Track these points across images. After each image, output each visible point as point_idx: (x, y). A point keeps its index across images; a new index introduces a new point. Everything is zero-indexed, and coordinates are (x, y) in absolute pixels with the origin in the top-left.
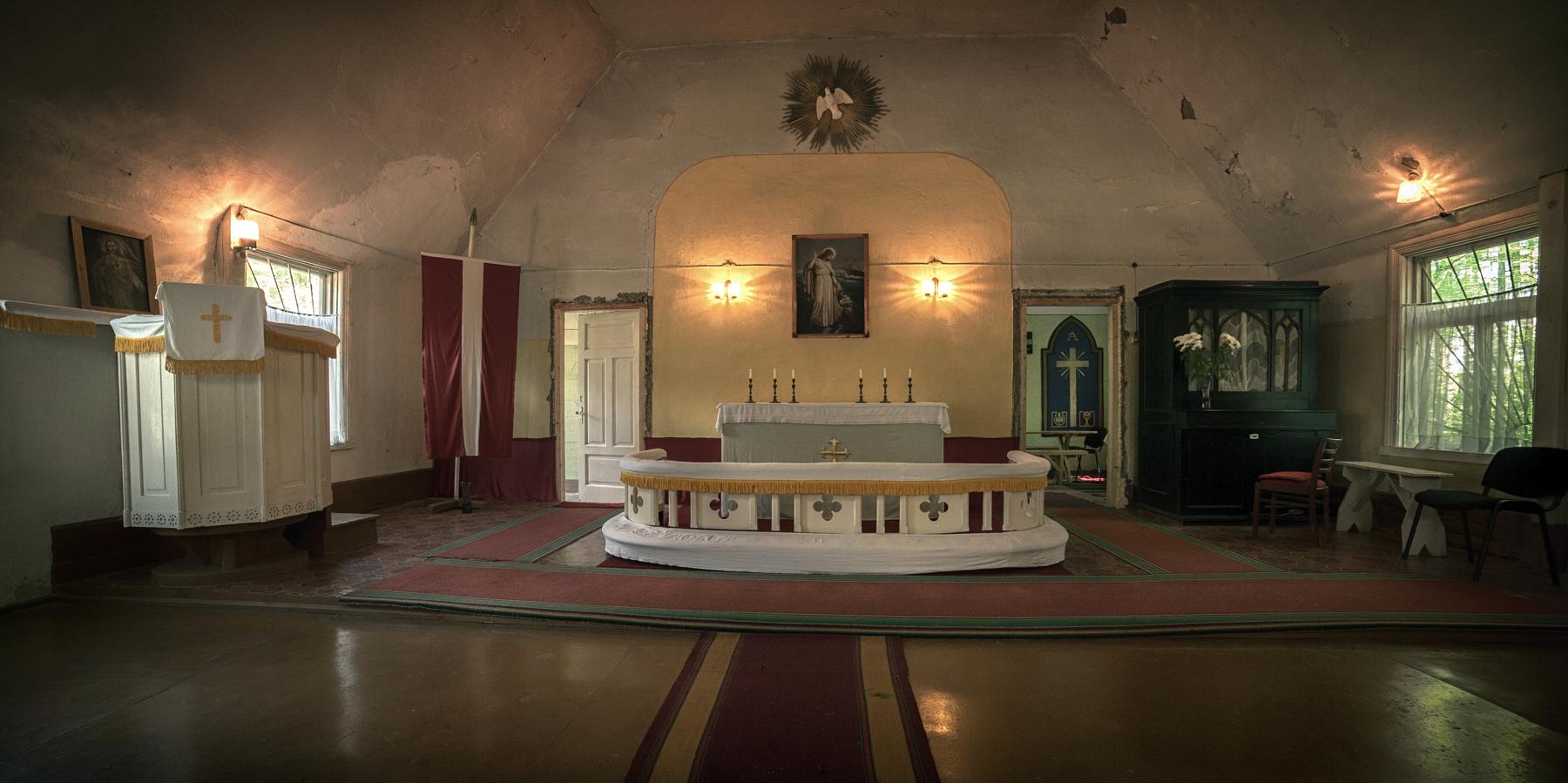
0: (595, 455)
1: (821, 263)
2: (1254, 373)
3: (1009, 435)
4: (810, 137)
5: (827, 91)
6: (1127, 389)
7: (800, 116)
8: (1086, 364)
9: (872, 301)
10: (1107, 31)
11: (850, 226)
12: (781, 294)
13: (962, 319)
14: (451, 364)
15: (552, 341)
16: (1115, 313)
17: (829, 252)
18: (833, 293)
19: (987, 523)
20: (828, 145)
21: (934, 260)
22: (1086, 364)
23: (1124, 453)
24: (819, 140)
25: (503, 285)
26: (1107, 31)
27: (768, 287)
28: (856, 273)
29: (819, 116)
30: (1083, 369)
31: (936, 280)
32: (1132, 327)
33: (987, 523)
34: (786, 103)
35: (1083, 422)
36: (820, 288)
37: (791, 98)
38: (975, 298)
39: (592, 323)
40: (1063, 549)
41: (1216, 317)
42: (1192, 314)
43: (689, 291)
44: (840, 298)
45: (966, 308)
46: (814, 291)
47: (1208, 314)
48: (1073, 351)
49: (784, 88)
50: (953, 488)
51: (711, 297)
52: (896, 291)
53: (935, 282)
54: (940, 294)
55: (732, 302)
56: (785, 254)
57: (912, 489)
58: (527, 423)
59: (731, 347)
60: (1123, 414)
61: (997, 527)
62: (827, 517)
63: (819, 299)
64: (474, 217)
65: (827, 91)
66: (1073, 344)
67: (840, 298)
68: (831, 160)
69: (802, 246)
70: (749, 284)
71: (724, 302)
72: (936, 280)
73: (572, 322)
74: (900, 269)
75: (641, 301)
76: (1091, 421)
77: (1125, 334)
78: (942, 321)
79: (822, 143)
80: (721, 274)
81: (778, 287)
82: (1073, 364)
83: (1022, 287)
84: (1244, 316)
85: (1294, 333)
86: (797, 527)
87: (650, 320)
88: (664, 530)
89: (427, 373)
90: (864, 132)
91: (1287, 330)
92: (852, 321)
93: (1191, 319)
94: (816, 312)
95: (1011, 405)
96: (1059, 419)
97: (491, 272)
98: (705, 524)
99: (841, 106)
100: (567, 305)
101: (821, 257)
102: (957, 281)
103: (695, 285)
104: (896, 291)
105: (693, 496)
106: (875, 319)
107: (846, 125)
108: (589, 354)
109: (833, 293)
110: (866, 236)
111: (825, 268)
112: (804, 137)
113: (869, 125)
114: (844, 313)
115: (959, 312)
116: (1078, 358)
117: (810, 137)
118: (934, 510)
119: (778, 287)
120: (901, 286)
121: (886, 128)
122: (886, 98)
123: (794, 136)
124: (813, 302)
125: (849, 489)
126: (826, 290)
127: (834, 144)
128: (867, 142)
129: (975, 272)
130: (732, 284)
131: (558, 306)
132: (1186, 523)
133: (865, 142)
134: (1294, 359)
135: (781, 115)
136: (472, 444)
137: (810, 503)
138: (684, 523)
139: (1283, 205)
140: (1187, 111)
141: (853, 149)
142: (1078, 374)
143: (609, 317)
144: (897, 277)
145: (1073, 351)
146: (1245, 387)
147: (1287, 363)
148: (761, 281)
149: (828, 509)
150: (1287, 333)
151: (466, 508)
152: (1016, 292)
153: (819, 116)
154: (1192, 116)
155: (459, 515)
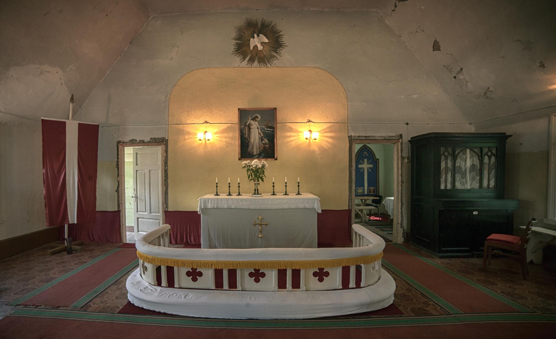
0: (139, 220)
1: (252, 122)
2: (473, 179)
3: (347, 208)
4: (247, 59)
5: (255, 35)
6: (404, 185)
7: (242, 48)
8: (371, 166)
9: (279, 141)
10: (396, 6)
11: (267, 104)
12: (232, 138)
13: (323, 150)
14: (60, 176)
15: (118, 162)
16: (397, 147)
17: (257, 117)
18: (259, 137)
19: (352, 284)
20: (256, 63)
21: (310, 121)
22: (371, 166)
23: (402, 217)
24: (252, 60)
25: (89, 134)
26: (396, 6)
27: (226, 135)
28: (270, 127)
29: (251, 48)
30: (370, 168)
31: (310, 131)
32: (405, 155)
33: (352, 284)
34: (234, 42)
35: (370, 192)
36: (252, 136)
37: (237, 39)
38: (329, 140)
39: (139, 152)
40: (393, 296)
41: (454, 151)
42: (442, 149)
43: (186, 137)
44: (262, 140)
45: (325, 145)
46: (249, 136)
47: (450, 150)
48: (366, 160)
49: (234, 34)
50: (334, 263)
51: (197, 139)
52: (291, 136)
53: (309, 132)
54: (313, 138)
55: (208, 142)
56: (235, 118)
57: (308, 265)
58: (104, 203)
59: (207, 165)
60: (402, 197)
61: (358, 286)
62: (257, 281)
63: (252, 141)
64: (72, 99)
65: (255, 35)
66: (365, 157)
67: (262, 140)
68: (257, 71)
69: (243, 113)
70: (216, 133)
71: (204, 142)
72: (310, 131)
73: (129, 153)
74: (293, 126)
75: (162, 142)
76: (373, 192)
77: (403, 158)
78: (314, 152)
79: (253, 62)
80: (203, 128)
81: (231, 135)
82: (366, 166)
83: (353, 135)
84: (468, 151)
85: (493, 159)
86: (239, 287)
87: (166, 151)
88: (159, 288)
89: (46, 182)
90: (279, 37)
91: (446, 159)
92: (269, 152)
93: (442, 153)
94: (250, 147)
95: (348, 194)
96: (360, 191)
97: (82, 128)
98: (183, 285)
99: (263, 44)
100: (125, 144)
101: (253, 119)
102: (321, 132)
103: (189, 133)
104: (291, 136)
105: (176, 269)
106: (280, 150)
107: (265, 53)
108: (137, 168)
109: (259, 137)
110: (276, 108)
111: (255, 125)
112: (244, 59)
113: (277, 53)
114: (264, 148)
115: (322, 147)
116: (368, 163)
117: (247, 59)
118: (321, 275)
119: (231, 135)
120: (293, 134)
121: (285, 55)
122: (285, 39)
123: (239, 58)
124: (249, 142)
125: (270, 265)
126: (255, 136)
127: (259, 62)
128: (275, 62)
129: (328, 128)
130: (208, 133)
131: (120, 145)
132: (441, 257)
133: (275, 62)
134: (493, 172)
135: (231, 45)
136: (73, 217)
137: (247, 273)
138: (171, 284)
139: (485, 94)
140: (436, 47)
141: (269, 65)
142: (368, 170)
143: (148, 150)
144: (291, 130)
145: (366, 160)
146: (468, 187)
147: (489, 174)
148: (223, 132)
149: (257, 275)
150: (490, 160)
151: (69, 251)
152: (350, 137)
153: (251, 48)
154: (439, 49)
155: (66, 257)
